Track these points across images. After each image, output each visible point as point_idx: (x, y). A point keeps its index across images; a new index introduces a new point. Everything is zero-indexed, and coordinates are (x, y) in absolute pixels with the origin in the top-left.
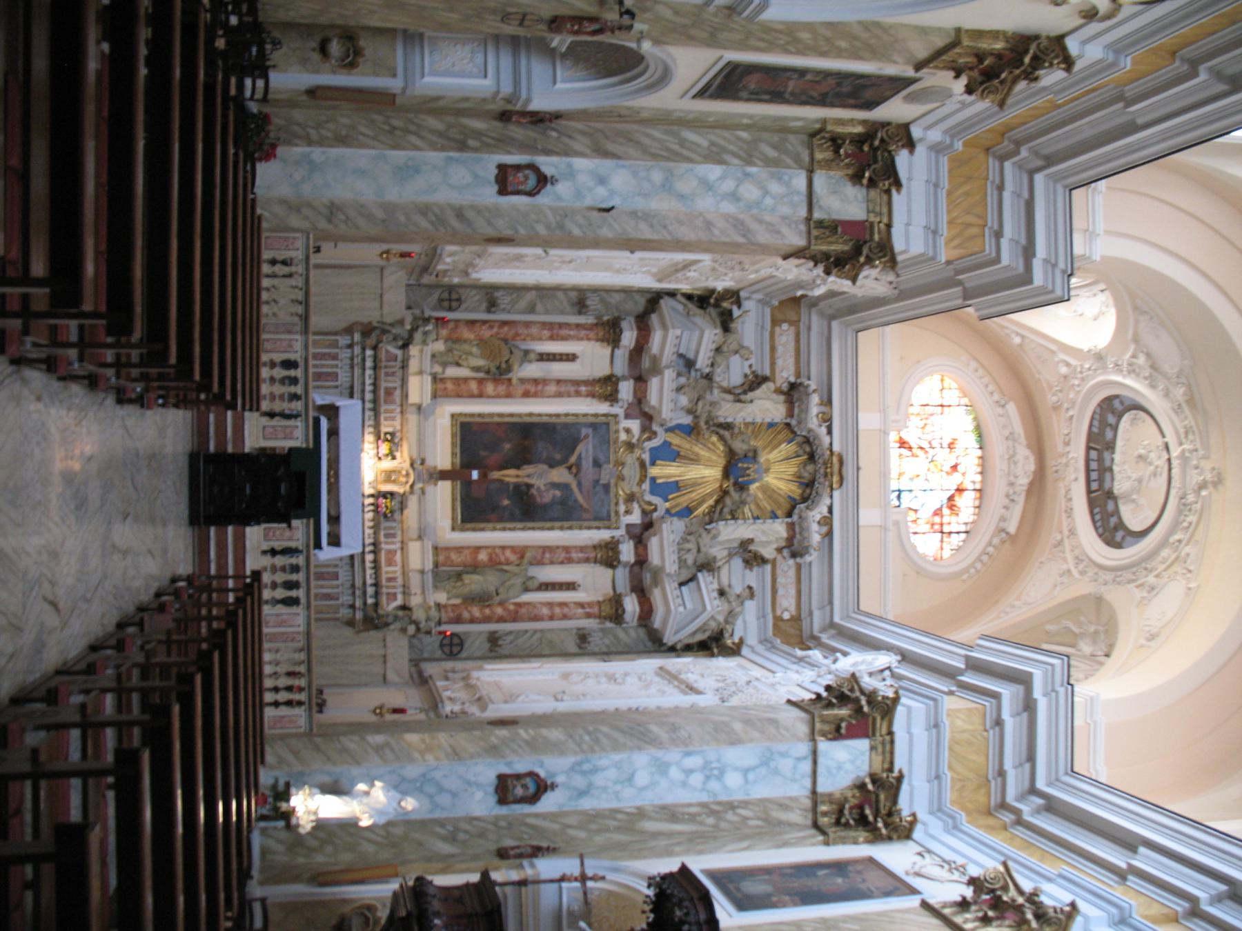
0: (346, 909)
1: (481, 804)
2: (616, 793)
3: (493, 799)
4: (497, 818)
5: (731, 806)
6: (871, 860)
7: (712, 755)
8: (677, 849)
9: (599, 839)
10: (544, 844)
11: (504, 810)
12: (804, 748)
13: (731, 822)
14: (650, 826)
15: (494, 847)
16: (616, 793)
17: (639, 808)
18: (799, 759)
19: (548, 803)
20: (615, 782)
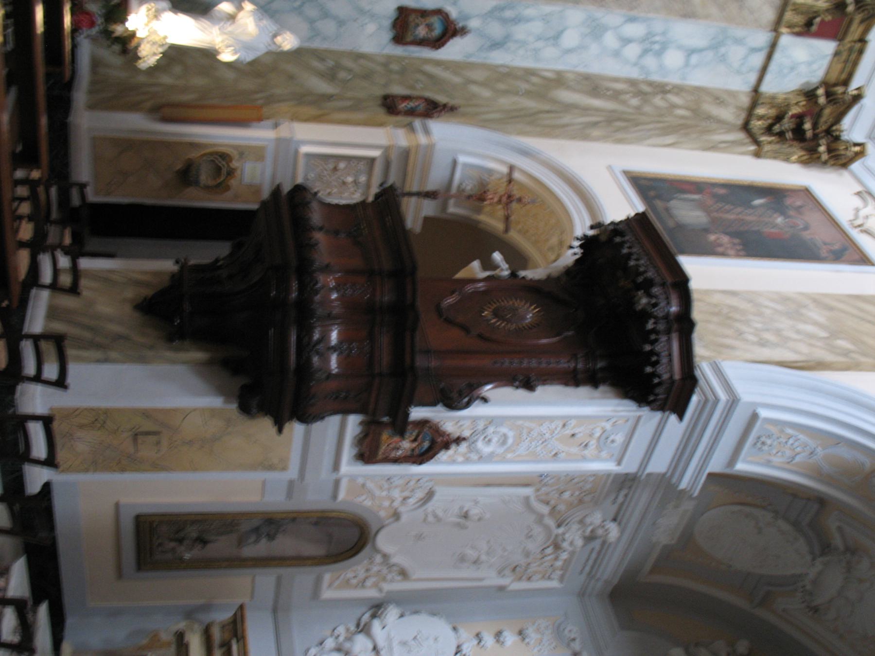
0: (194, 155)
1: (373, 39)
2: (536, 51)
3: (387, 35)
4: (390, 59)
5: (662, 89)
6: (807, 192)
7: (658, 26)
8: (596, 133)
9: (505, 102)
10: (441, 99)
11: (399, 51)
12: (762, 38)
13: (657, 108)
14: (565, 96)
15: (379, 92)
16: (536, 51)
17: (559, 73)
18: (754, 50)
19: (454, 50)
20: (539, 38)
